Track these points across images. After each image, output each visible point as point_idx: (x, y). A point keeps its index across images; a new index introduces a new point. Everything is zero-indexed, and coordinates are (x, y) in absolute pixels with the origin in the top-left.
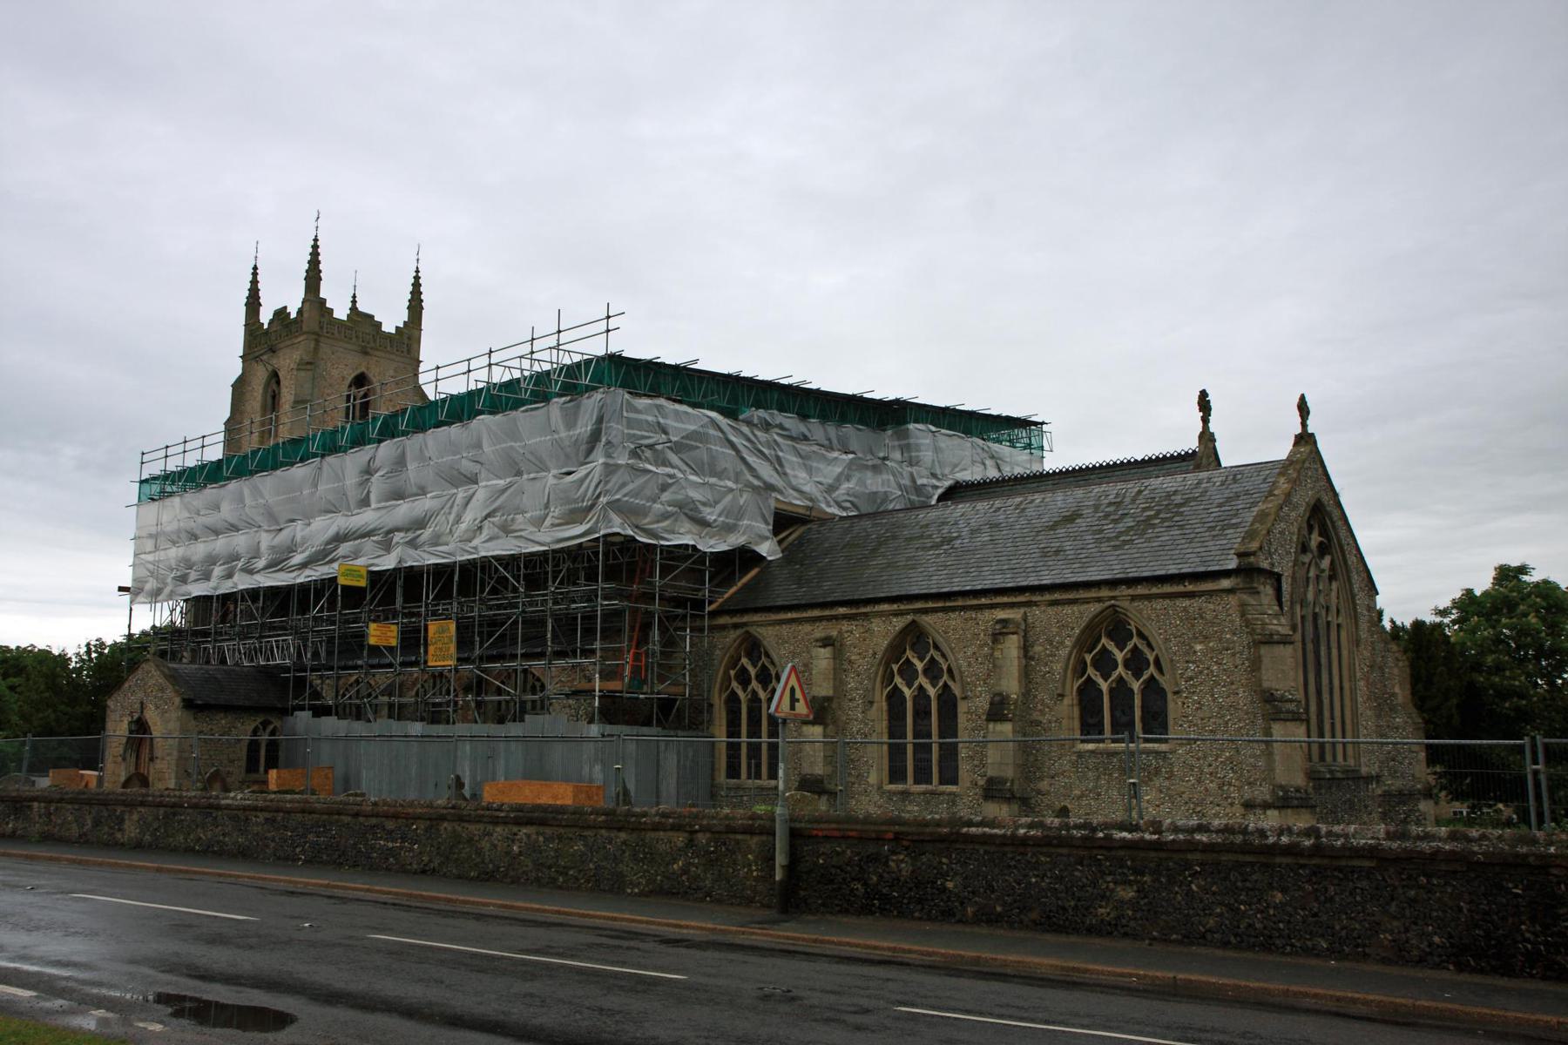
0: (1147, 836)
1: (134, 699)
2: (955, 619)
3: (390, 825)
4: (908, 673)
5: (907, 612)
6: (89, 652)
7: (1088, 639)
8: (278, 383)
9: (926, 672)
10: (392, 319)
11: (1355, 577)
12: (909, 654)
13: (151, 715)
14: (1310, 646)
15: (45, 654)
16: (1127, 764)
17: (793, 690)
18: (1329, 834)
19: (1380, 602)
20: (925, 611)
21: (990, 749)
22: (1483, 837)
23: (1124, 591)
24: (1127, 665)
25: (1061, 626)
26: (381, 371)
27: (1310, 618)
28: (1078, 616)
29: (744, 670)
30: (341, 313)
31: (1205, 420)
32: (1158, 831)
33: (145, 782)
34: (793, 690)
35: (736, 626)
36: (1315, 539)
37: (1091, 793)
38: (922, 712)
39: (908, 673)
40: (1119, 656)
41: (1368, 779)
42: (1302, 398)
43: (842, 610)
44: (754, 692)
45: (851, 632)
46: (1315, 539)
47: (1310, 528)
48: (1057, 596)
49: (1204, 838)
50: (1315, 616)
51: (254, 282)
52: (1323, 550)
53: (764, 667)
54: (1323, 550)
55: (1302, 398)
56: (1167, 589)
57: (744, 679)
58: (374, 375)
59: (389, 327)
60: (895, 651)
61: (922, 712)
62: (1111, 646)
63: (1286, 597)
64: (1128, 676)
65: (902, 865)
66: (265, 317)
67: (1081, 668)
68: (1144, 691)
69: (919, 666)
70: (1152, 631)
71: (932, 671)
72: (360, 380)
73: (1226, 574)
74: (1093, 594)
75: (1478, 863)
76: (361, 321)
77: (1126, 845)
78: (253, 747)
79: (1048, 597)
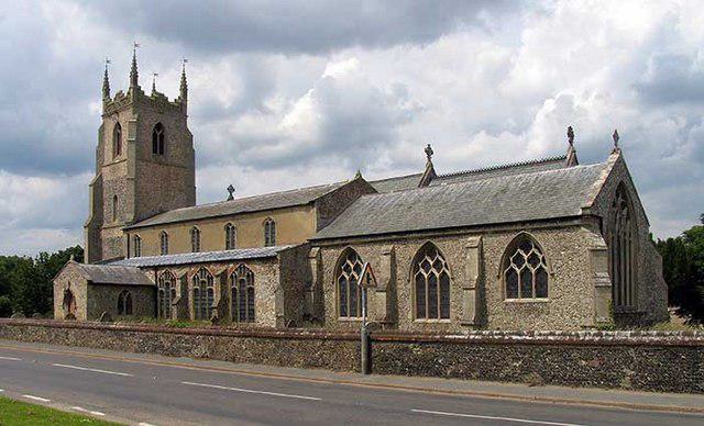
0: (528, 338)
1: (65, 281)
2: (551, 236)
3: (187, 337)
4: (426, 266)
5: (426, 237)
6: (41, 258)
7: (511, 250)
8: (120, 128)
9: (434, 266)
10: (173, 95)
11: (639, 218)
12: (348, 261)
13: (73, 288)
14: (616, 252)
15: (21, 261)
16: (531, 309)
17: (368, 275)
18: (607, 335)
19: (651, 230)
20: (435, 237)
21: (463, 304)
22: (671, 334)
23: (528, 226)
24: (529, 262)
25: (498, 244)
26: (169, 123)
27: (616, 239)
28: (505, 240)
29: (348, 266)
30: (148, 93)
31: (429, 158)
32: (532, 334)
33: (74, 317)
34: (368, 275)
35: (344, 245)
36: (620, 200)
37: (511, 319)
38: (433, 285)
39: (426, 266)
40: (526, 257)
41: (641, 314)
42: (570, 128)
43: (394, 237)
44: (353, 276)
45: (400, 249)
46: (620, 200)
47: (617, 196)
48: (496, 229)
49: (551, 338)
50: (619, 237)
51: (135, 64)
52: (624, 205)
53: (438, 261)
54: (624, 205)
55: (570, 128)
56: (549, 225)
57: (347, 269)
58: (165, 125)
59: (171, 100)
60: (420, 256)
61: (433, 285)
62: (522, 252)
63: (604, 228)
64: (529, 266)
65: (417, 351)
66: (112, 95)
67: (416, 269)
68: (537, 274)
69: (352, 266)
70: (542, 244)
71: (437, 265)
72: (159, 126)
73: (577, 217)
74: (514, 228)
75: (668, 346)
76: (160, 99)
77: (518, 342)
78: (120, 300)
79: (493, 229)
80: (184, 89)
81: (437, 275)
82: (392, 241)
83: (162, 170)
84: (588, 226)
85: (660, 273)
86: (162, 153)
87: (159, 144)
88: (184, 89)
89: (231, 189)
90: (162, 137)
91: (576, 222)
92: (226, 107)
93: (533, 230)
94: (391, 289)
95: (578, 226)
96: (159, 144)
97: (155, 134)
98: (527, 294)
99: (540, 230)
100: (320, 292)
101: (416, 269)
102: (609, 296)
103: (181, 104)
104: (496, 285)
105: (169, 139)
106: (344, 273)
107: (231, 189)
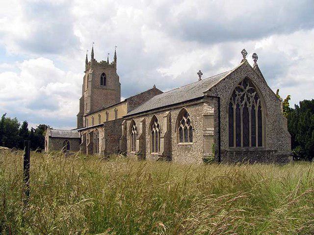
10: (111, 61)
23: (185, 104)
26: (108, 73)
69: (186, 120)
72: (104, 74)
73: (202, 98)
80: (108, 60)
81: (183, 128)
82: (142, 116)
83: (105, 91)
84: (207, 102)
85: (285, 128)
86: (105, 85)
87: (103, 80)
88: (108, 60)
89: (200, 74)
90: (105, 78)
91: (202, 101)
92: (146, 50)
93: (187, 106)
94: (143, 138)
95: (203, 103)
96: (103, 80)
97: (102, 78)
98: (186, 141)
99: (190, 106)
100: (125, 139)
101: (179, 125)
102: (212, 141)
103: (114, 64)
104: (175, 135)
105: (108, 79)
106: (182, 125)
107: (200, 74)
